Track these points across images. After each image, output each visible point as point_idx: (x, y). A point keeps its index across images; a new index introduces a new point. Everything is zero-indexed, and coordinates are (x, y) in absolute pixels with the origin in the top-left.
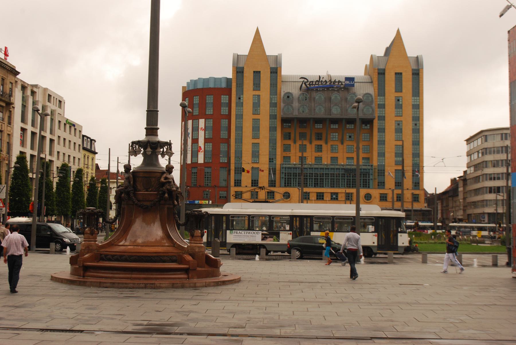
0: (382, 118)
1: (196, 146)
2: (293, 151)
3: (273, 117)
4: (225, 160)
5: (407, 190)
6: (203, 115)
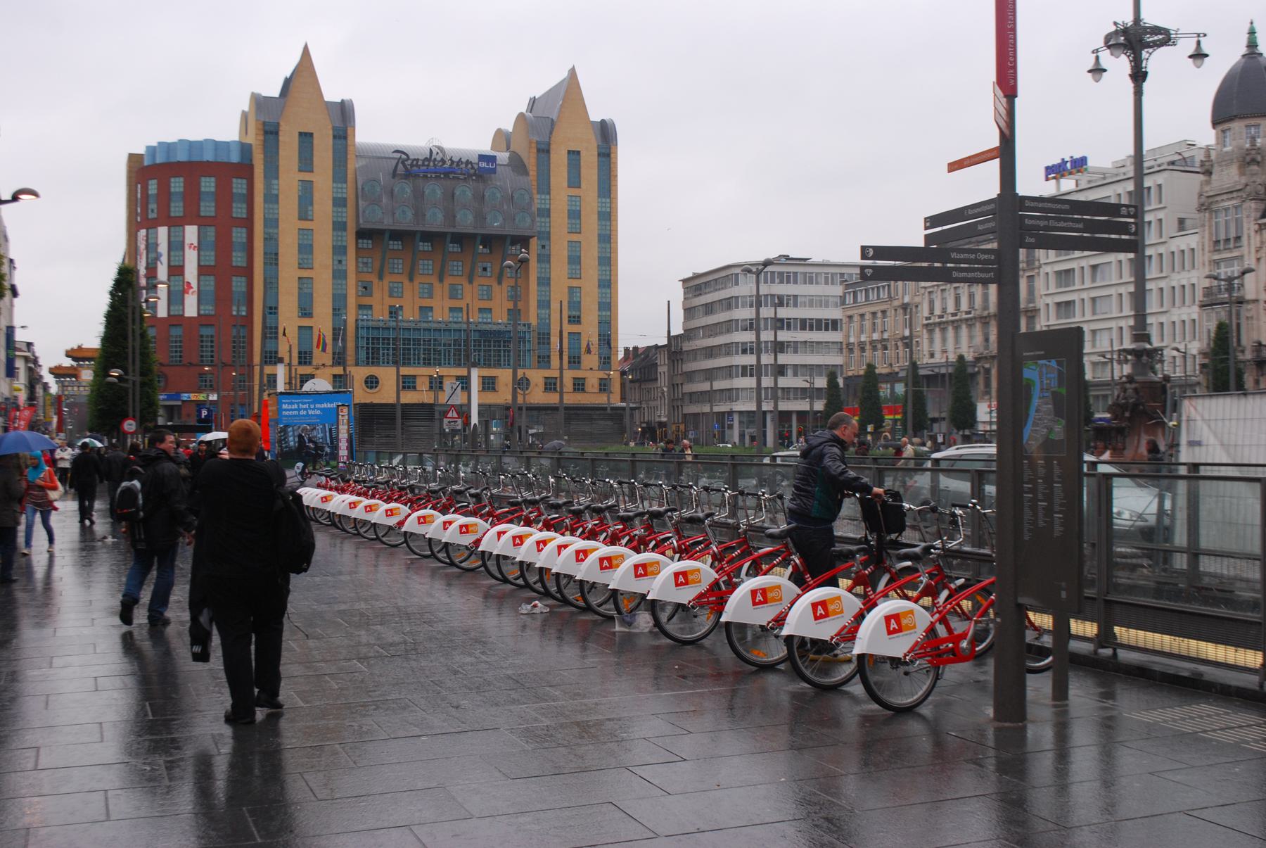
0: (547, 236)
3: (339, 226)
6: (192, 216)
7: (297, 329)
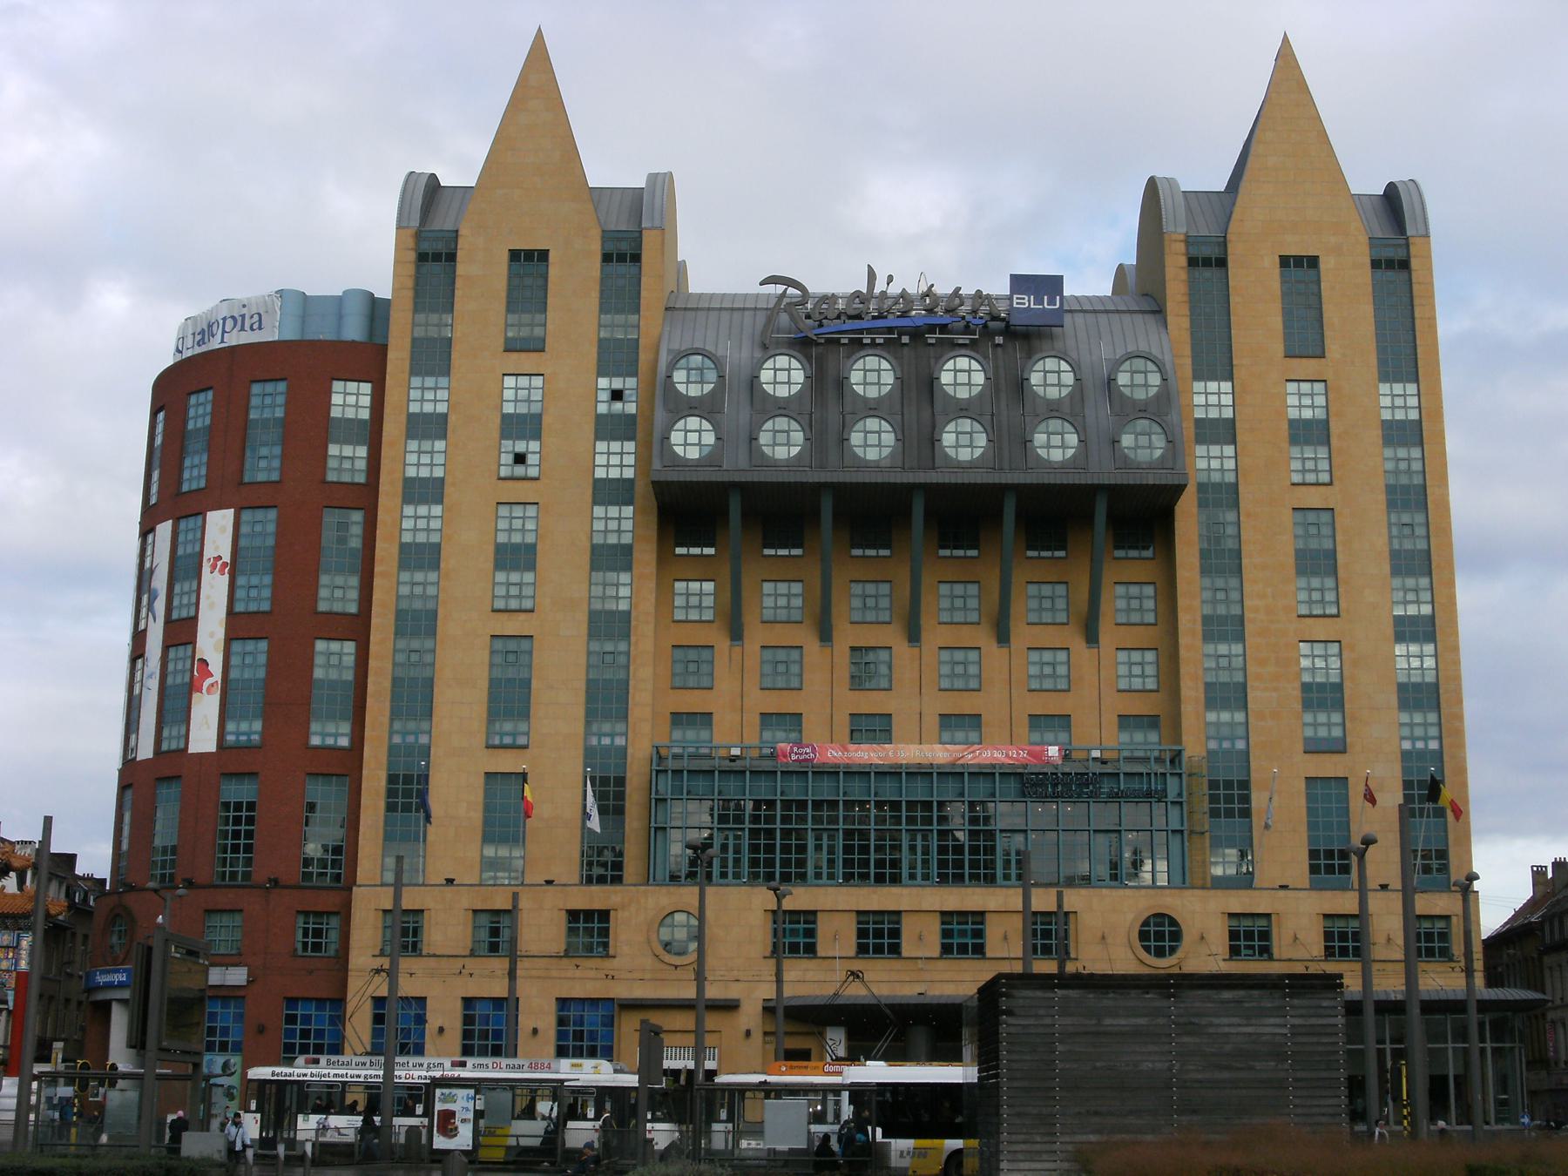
1: (184, 659)
2: (816, 680)
4: (336, 735)
5: (549, 888)
7: (481, 780)
